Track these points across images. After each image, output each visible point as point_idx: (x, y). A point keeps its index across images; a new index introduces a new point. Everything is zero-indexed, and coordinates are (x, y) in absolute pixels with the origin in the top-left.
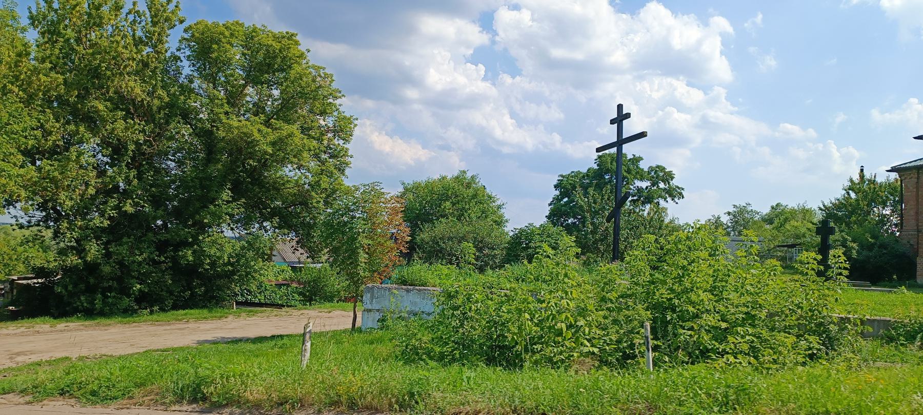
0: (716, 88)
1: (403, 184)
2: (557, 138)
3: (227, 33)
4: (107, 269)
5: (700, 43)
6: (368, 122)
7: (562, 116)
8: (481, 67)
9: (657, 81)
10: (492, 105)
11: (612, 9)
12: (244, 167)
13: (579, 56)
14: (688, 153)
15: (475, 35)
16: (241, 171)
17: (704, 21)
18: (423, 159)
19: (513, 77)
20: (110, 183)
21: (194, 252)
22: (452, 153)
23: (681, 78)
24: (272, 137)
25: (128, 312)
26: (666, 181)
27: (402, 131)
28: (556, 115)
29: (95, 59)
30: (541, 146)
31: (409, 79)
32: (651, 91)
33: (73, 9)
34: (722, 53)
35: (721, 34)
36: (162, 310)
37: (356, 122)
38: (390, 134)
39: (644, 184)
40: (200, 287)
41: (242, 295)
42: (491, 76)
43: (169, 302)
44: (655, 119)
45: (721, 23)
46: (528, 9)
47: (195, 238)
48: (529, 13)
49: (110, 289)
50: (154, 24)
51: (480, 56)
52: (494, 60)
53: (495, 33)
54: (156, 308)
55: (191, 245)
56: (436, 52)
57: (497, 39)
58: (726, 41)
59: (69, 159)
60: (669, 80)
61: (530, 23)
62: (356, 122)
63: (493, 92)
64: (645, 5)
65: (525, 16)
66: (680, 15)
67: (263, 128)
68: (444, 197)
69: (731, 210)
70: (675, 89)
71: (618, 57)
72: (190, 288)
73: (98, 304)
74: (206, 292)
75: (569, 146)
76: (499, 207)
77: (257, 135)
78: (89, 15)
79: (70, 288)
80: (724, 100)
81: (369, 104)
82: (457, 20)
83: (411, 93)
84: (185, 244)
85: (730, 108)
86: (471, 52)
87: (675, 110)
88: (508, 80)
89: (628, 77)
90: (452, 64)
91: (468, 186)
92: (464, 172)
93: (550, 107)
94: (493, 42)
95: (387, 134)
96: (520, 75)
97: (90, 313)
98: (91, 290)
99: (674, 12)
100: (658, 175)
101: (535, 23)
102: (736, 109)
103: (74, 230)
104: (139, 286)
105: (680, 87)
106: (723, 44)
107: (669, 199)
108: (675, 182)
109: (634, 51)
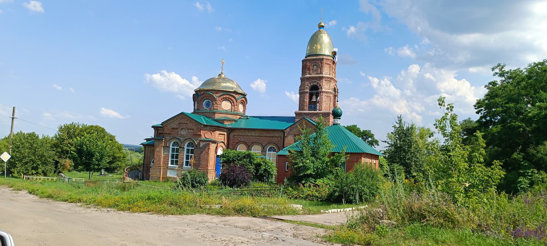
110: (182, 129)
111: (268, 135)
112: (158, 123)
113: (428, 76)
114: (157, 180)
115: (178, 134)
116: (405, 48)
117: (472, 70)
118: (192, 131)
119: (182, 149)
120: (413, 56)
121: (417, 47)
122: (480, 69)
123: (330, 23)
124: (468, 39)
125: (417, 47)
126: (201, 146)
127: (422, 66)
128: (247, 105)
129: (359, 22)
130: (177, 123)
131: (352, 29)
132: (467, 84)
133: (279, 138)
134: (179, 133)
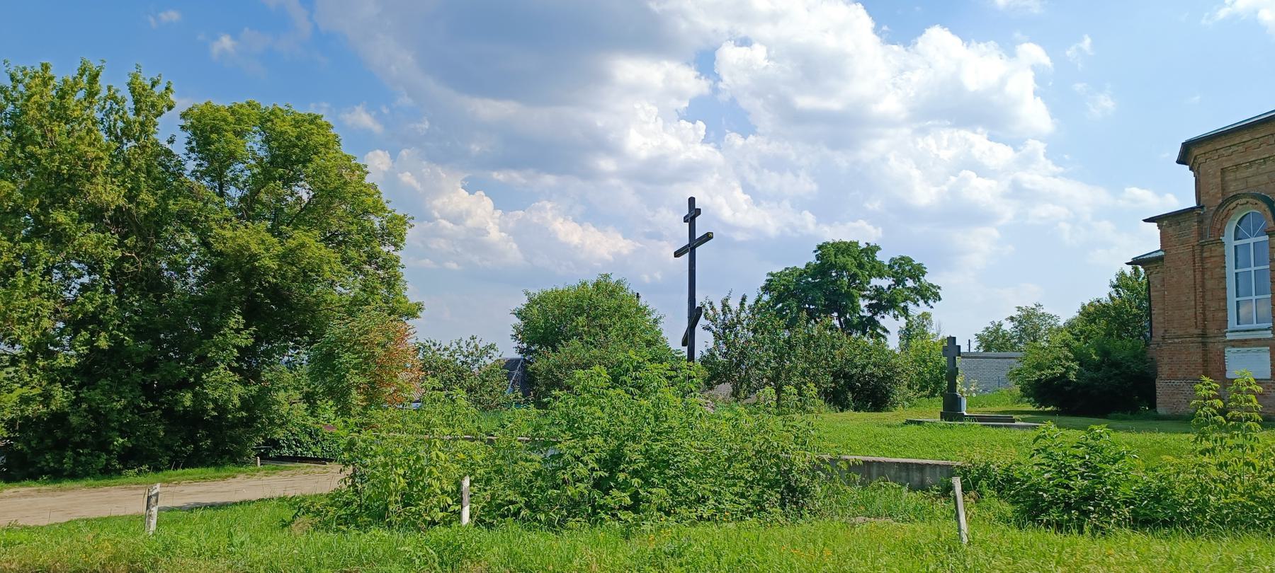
0: (1030, 141)
1: (527, 294)
2: (809, 218)
3: (231, 119)
4: (74, 420)
5: (1003, 82)
6: (549, 206)
7: (815, 187)
8: (701, 125)
9: (946, 134)
10: (716, 176)
11: (878, 39)
12: (261, 284)
13: (834, 105)
14: (995, 233)
15: (689, 81)
16: (258, 290)
17: (1009, 50)
18: (625, 252)
19: (745, 137)
20: (78, 312)
21: (195, 395)
22: (664, 243)
23: (980, 130)
24: (279, 249)
25: (107, 472)
26: (915, 277)
27: (593, 216)
28: (807, 186)
29: (53, 161)
30: (787, 229)
31: (602, 144)
32: (938, 149)
33: (28, 100)
34: (1036, 93)
35: (1033, 68)
36: (157, 469)
37: (411, 222)
38: (580, 221)
39: (885, 283)
40: (213, 441)
41: (289, 447)
42: (714, 136)
43: (165, 460)
44: (945, 188)
45: (1033, 52)
46: (762, 43)
47: (198, 378)
48: (764, 49)
49: (83, 444)
50: (137, 112)
51: (698, 110)
52: (718, 115)
53: (718, 78)
54: (145, 467)
55: (190, 387)
56: (637, 106)
57: (721, 85)
58: (1041, 77)
59: (15, 286)
60: (963, 133)
61: (765, 63)
62: (411, 222)
63: (718, 158)
64: (922, 32)
65: (758, 54)
66: (974, 43)
67: (268, 236)
68: (578, 310)
69: (1015, 313)
70: (971, 146)
71: (890, 105)
72: (195, 442)
73: (68, 464)
74: (216, 445)
75: (826, 228)
76: (656, 321)
77: (254, 248)
78: (53, 105)
79: (33, 444)
80: (1043, 159)
81: (550, 180)
82: (666, 63)
83: (606, 164)
84: (184, 385)
85: (1052, 168)
86: (686, 104)
87: (973, 174)
88: (737, 140)
89: (906, 131)
90: (660, 121)
91: (612, 294)
92: (607, 276)
93: (797, 176)
94: (715, 90)
95: (575, 220)
96: (755, 133)
97: (57, 475)
98: (60, 446)
99: (966, 39)
100: (903, 271)
101: (772, 63)
102: (1061, 169)
103: (35, 372)
104: (121, 440)
105: (978, 142)
106: (1037, 80)
107: (921, 302)
108: (928, 279)
109: (912, 94)
113: (407, 178)
114: (1182, 420)
116: (359, 109)
117: (499, 176)
120: (377, 128)
121: (385, 111)
122: (515, 175)
123: (163, 16)
124: (489, 109)
125: (385, 111)
127: (394, 155)
129: (246, 29)
131: (226, 42)
132: (488, 203)
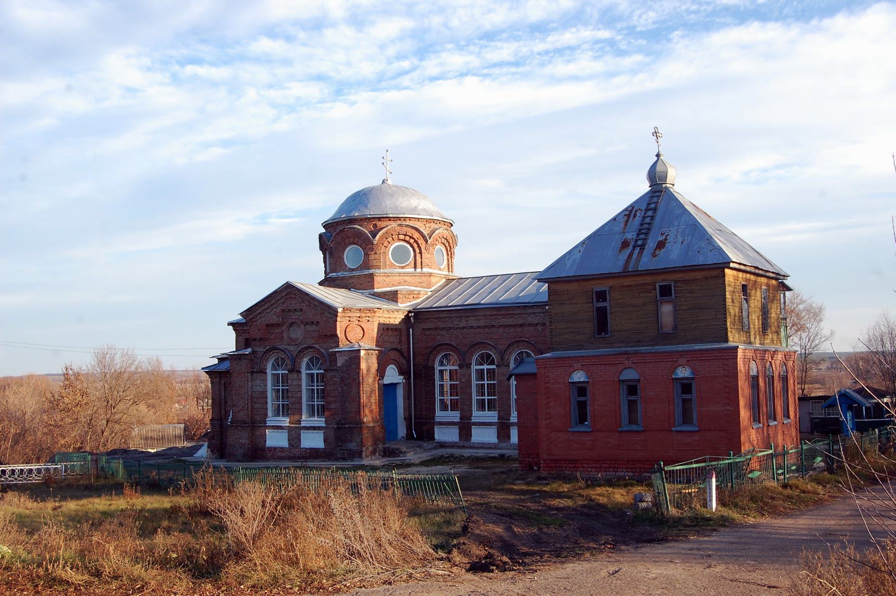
110: (292, 324)
111: (510, 321)
112: (237, 317)
115: (282, 338)
118: (314, 328)
119: (295, 375)
126: (339, 364)
128: (457, 250)
130: (278, 310)
133: (540, 328)
134: (285, 335)
